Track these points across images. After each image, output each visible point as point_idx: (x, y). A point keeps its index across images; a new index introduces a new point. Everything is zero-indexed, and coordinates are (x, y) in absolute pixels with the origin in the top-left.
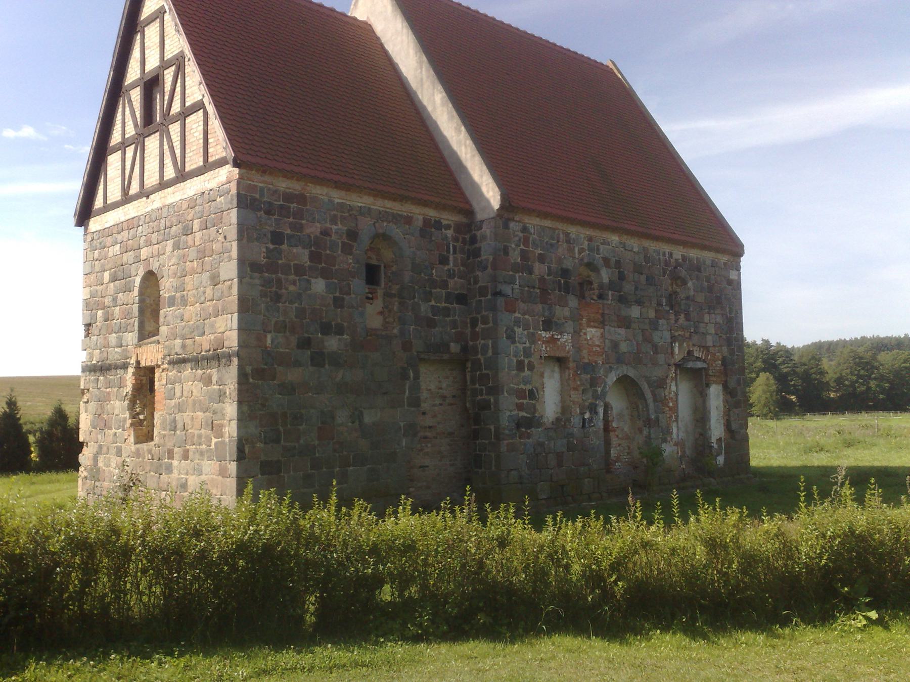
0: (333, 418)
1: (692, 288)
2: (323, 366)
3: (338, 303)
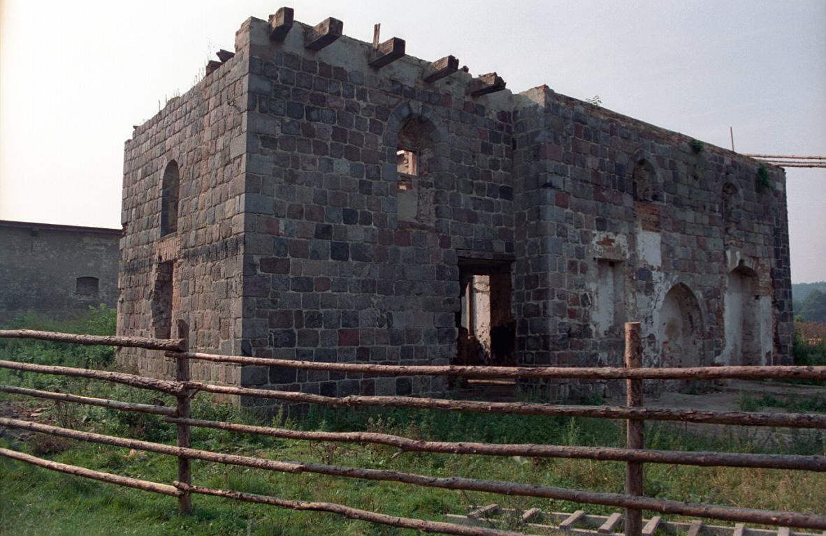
0: (356, 320)
1: (742, 195)
2: (346, 259)
3: (365, 187)
